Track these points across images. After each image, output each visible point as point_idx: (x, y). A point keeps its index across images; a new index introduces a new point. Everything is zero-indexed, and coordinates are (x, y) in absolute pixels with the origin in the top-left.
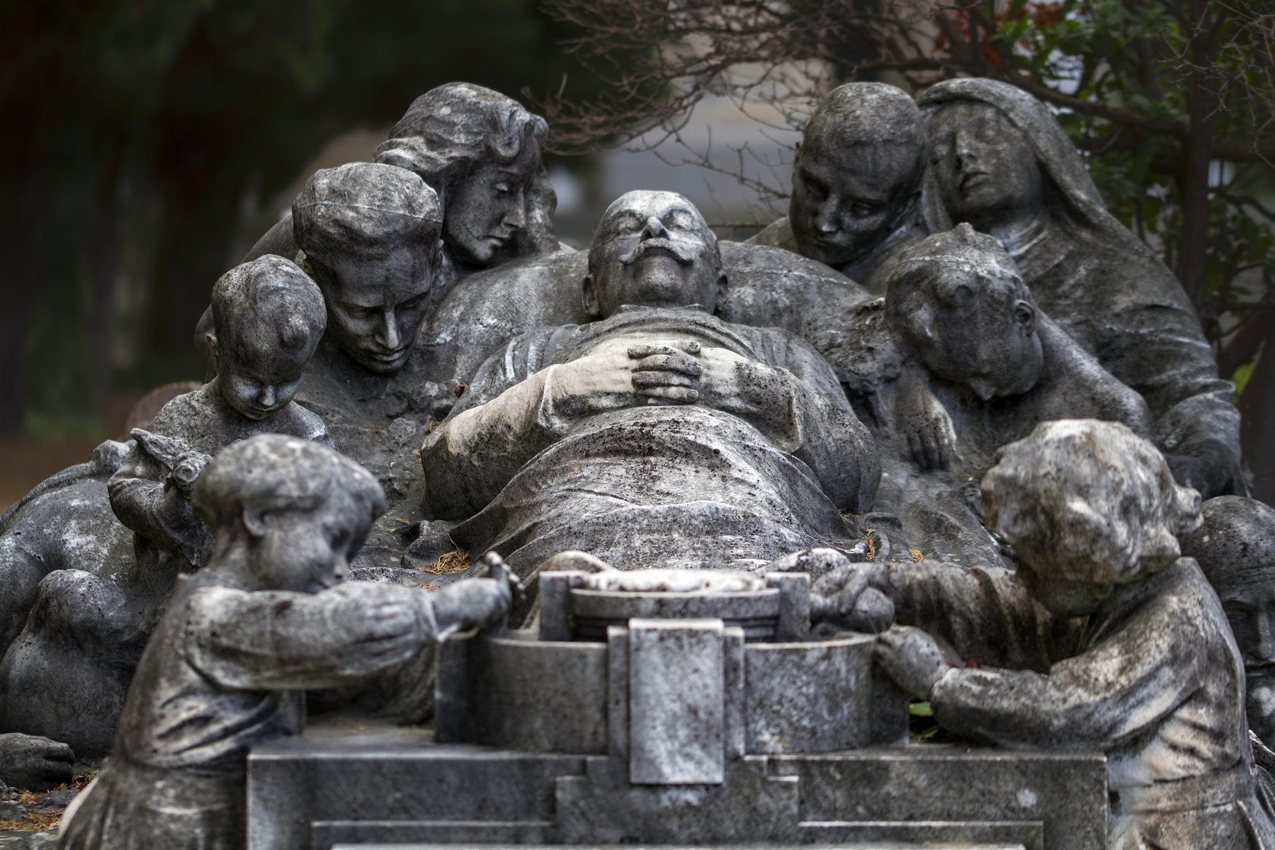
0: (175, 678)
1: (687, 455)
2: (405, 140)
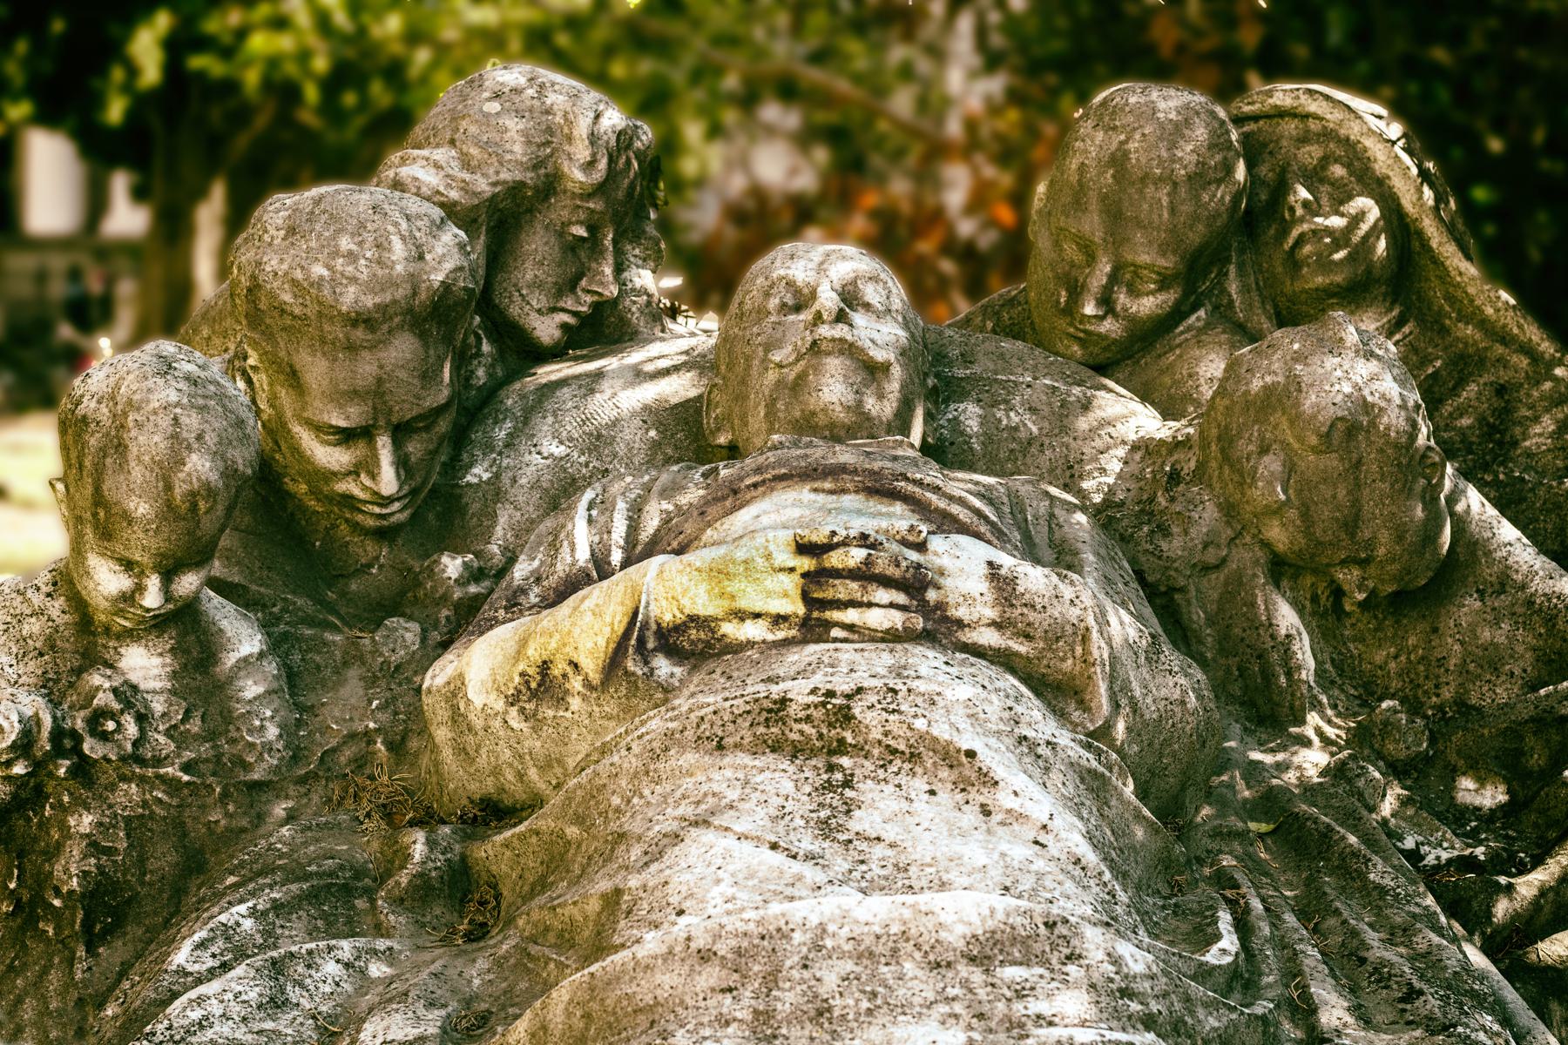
1: (914, 757)
2: (425, 152)
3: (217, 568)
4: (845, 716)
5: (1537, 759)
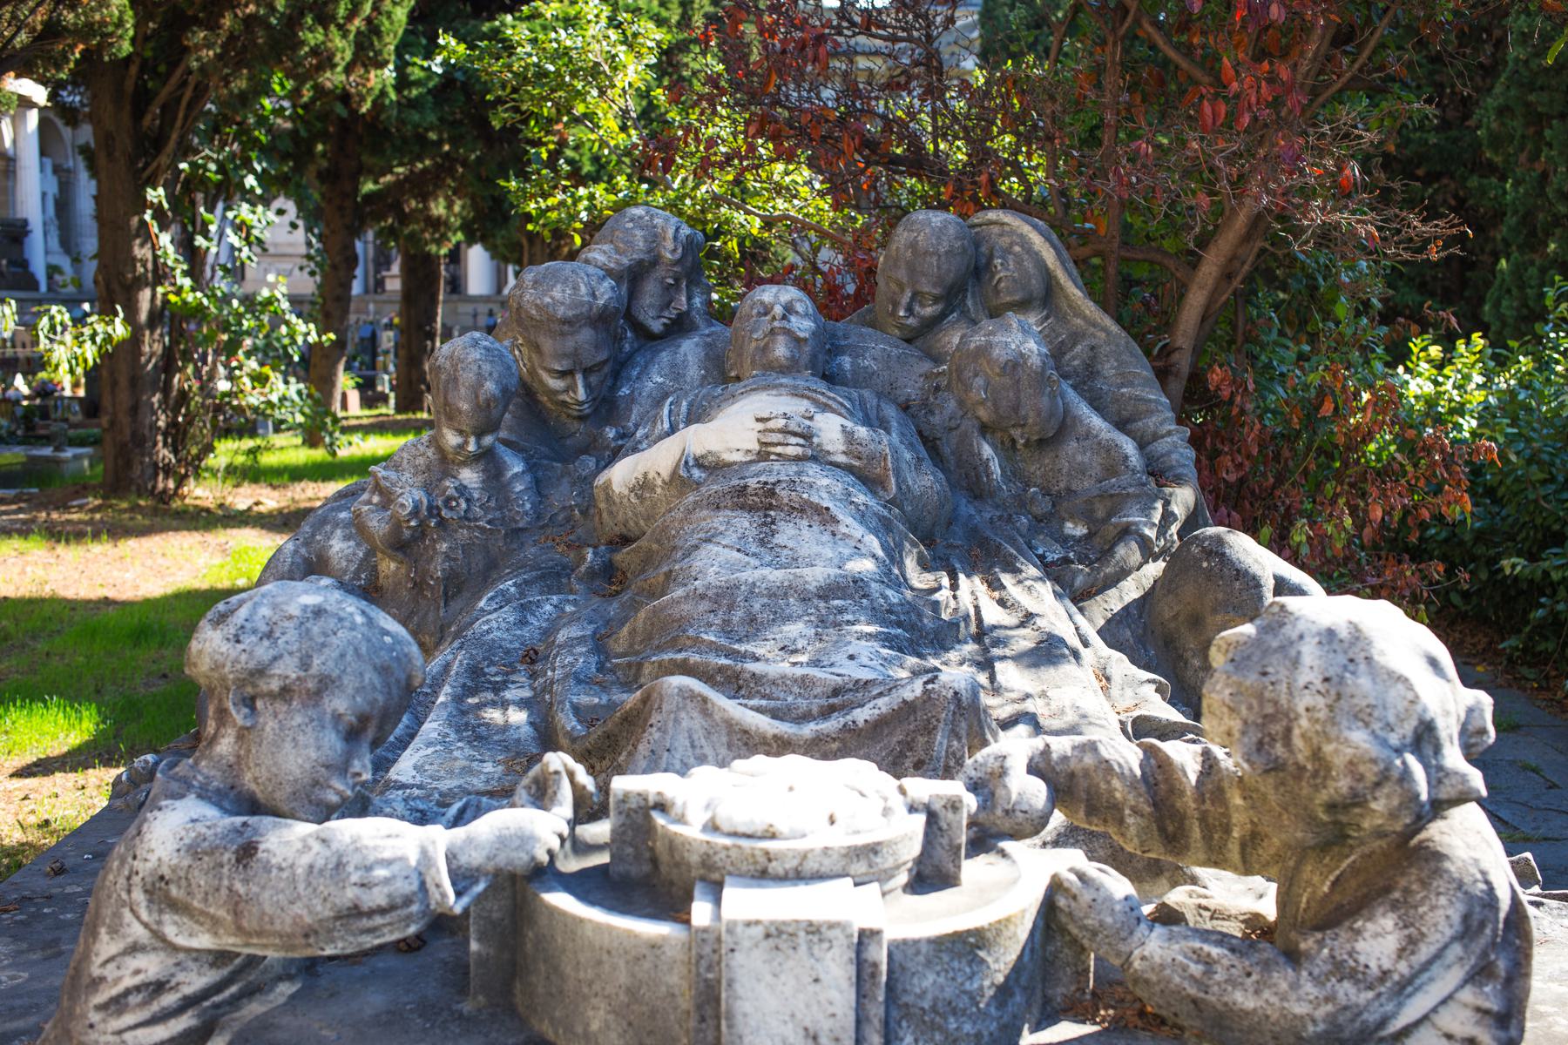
0: (114, 931)
1: (802, 511)
3: (503, 434)
4: (772, 493)
5: (1100, 514)
